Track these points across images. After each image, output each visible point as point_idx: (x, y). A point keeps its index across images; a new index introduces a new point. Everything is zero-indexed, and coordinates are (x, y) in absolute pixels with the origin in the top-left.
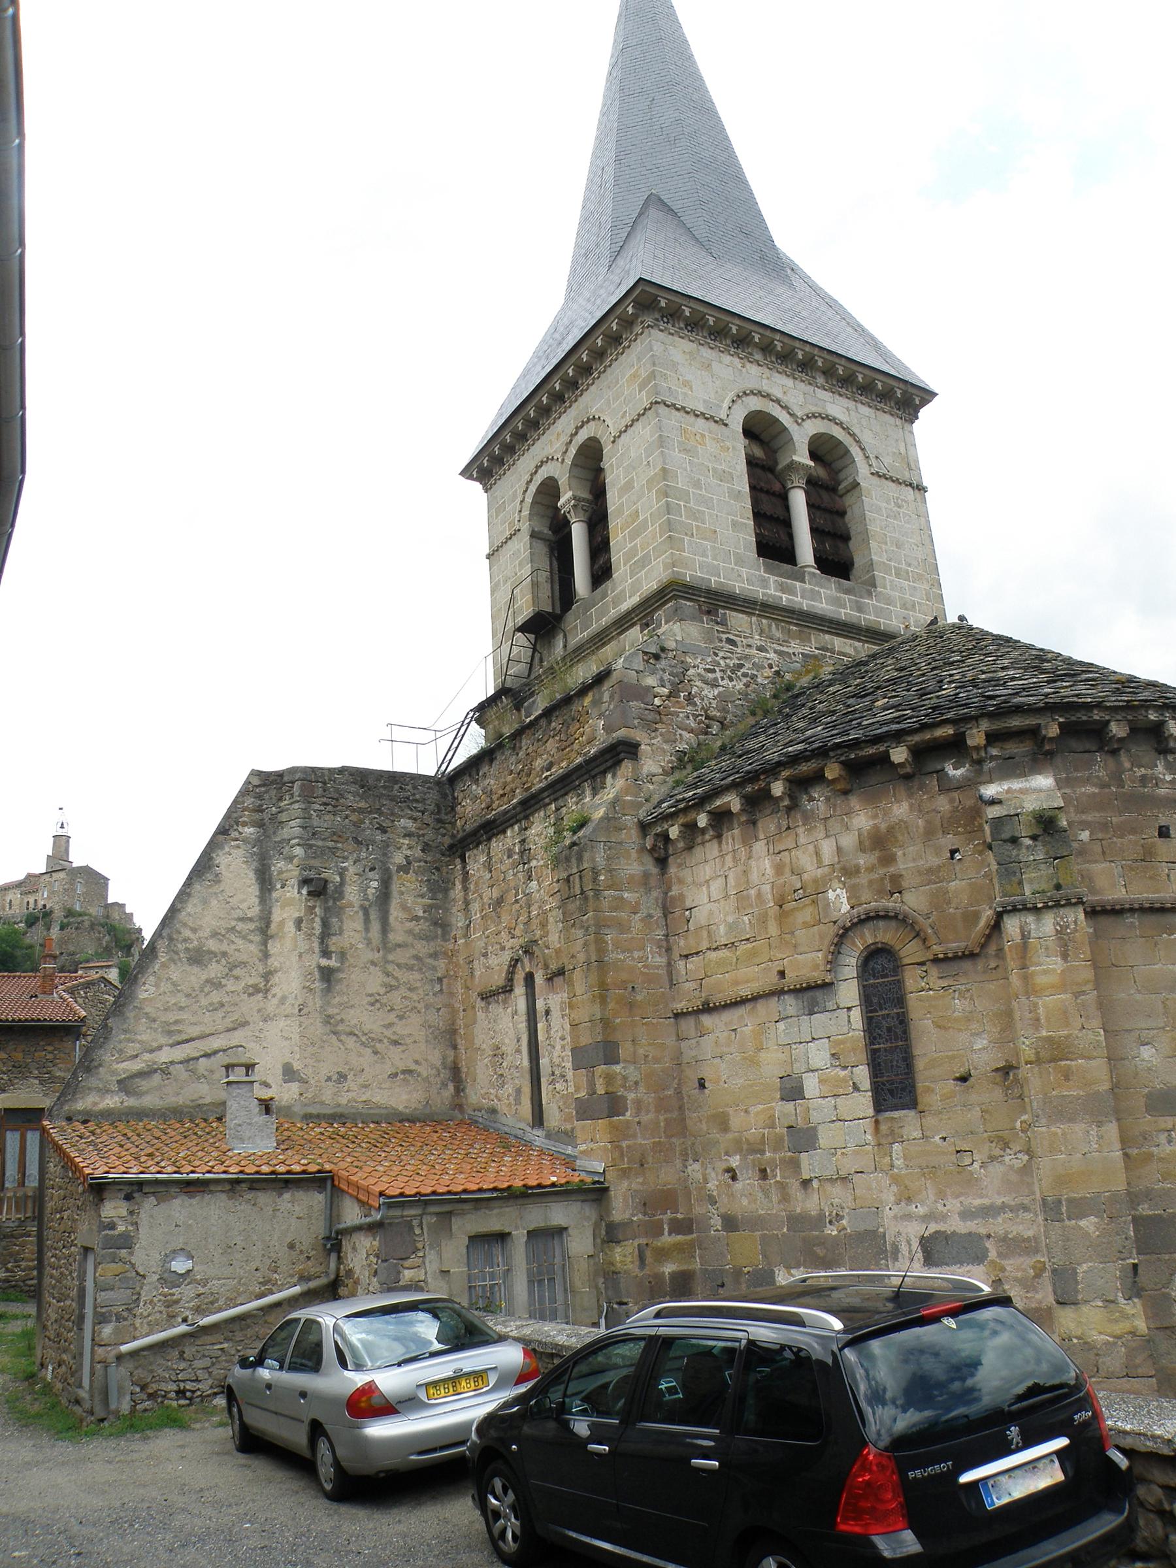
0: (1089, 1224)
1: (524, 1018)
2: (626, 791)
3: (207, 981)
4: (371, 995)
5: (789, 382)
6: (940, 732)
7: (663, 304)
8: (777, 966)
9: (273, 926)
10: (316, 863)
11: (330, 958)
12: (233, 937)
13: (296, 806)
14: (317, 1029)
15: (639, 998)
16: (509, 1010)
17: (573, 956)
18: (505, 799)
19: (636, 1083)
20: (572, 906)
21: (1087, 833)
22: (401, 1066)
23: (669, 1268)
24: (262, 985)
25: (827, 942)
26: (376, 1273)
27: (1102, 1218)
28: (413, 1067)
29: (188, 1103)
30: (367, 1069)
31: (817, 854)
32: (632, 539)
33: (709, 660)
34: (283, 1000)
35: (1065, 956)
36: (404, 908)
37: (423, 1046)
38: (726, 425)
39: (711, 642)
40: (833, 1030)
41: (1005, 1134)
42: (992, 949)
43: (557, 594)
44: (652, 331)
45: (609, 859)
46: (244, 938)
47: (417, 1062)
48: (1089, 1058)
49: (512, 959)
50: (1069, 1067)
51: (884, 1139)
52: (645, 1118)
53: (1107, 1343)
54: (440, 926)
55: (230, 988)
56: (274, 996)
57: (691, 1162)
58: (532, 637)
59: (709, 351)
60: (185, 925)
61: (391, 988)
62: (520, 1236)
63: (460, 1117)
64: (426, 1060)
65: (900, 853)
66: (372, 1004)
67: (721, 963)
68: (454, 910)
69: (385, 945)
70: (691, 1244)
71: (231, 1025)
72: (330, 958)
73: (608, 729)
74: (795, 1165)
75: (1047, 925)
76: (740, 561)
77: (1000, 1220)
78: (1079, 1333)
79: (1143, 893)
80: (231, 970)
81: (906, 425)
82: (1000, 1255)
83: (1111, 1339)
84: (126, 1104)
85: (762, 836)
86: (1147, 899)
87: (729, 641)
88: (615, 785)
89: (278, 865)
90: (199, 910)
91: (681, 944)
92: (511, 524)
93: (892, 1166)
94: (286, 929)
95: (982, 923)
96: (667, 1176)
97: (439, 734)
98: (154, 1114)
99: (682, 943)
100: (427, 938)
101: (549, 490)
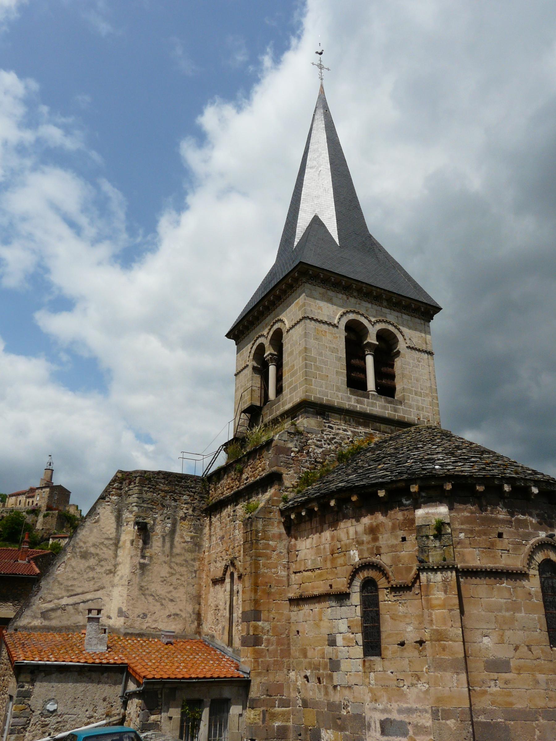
0: (451, 723)
1: (229, 593)
2: (275, 495)
3: (88, 567)
4: (162, 577)
5: (369, 305)
7: (311, 273)
8: (329, 582)
9: (121, 543)
10: (143, 515)
11: (145, 559)
12: (102, 547)
13: (136, 488)
14: (136, 592)
15: (273, 590)
17: (246, 569)
18: (229, 490)
19: (268, 631)
20: (247, 546)
21: (463, 534)
22: (173, 612)
23: (277, 724)
24: (113, 570)
25: (348, 575)
27: (457, 721)
28: (179, 612)
29: (73, 624)
30: (157, 612)
31: (348, 533)
33: (319, 435)
34: (122, 577)
35: (445, 592)
36: (182, 537)
39: (321, 427)
40: (349, 615)
41: (419, 673)
43: (263, 395)
45: (264, 526)
46: (107, 547)
47: (181, 610)
48: (455, 641)
49: (226, 565)
50: (445, 644)
51: (368, 668)
52: (271, 648)
54: (197, 545)
55: (98, 570)
56: (118, 575)
57: (291, 670)
59: (332, 292)
60: (81, 540)
61: (172, 574)
62: (207, 701)
63: (199, 638)
65: (380, 537)
66: (162, 582)
67: (309, 577)
68: (205, 539)
69: (171, 554)
70: (288, 713)
71: (96, 588)
72: (145, 559)
73: (270, 466)
74: (331, 677)
75: (439, 577)
76: (338, 389)
77: (415, 716)
80: (99, 562)
81: (426, 323)
82: (414, 733)
84: (43, 624)
85: (327, 522)
86: (489, 567)
88: (270, 492)
89: (126, 515)
90: (88, 533)
91: (294, 567)
93: (370, 683)
94: (126, 545)
96: (279, 677)
97: (204, 457)
98: (56, 630)
99: (294, 567)
101: (261, 348)
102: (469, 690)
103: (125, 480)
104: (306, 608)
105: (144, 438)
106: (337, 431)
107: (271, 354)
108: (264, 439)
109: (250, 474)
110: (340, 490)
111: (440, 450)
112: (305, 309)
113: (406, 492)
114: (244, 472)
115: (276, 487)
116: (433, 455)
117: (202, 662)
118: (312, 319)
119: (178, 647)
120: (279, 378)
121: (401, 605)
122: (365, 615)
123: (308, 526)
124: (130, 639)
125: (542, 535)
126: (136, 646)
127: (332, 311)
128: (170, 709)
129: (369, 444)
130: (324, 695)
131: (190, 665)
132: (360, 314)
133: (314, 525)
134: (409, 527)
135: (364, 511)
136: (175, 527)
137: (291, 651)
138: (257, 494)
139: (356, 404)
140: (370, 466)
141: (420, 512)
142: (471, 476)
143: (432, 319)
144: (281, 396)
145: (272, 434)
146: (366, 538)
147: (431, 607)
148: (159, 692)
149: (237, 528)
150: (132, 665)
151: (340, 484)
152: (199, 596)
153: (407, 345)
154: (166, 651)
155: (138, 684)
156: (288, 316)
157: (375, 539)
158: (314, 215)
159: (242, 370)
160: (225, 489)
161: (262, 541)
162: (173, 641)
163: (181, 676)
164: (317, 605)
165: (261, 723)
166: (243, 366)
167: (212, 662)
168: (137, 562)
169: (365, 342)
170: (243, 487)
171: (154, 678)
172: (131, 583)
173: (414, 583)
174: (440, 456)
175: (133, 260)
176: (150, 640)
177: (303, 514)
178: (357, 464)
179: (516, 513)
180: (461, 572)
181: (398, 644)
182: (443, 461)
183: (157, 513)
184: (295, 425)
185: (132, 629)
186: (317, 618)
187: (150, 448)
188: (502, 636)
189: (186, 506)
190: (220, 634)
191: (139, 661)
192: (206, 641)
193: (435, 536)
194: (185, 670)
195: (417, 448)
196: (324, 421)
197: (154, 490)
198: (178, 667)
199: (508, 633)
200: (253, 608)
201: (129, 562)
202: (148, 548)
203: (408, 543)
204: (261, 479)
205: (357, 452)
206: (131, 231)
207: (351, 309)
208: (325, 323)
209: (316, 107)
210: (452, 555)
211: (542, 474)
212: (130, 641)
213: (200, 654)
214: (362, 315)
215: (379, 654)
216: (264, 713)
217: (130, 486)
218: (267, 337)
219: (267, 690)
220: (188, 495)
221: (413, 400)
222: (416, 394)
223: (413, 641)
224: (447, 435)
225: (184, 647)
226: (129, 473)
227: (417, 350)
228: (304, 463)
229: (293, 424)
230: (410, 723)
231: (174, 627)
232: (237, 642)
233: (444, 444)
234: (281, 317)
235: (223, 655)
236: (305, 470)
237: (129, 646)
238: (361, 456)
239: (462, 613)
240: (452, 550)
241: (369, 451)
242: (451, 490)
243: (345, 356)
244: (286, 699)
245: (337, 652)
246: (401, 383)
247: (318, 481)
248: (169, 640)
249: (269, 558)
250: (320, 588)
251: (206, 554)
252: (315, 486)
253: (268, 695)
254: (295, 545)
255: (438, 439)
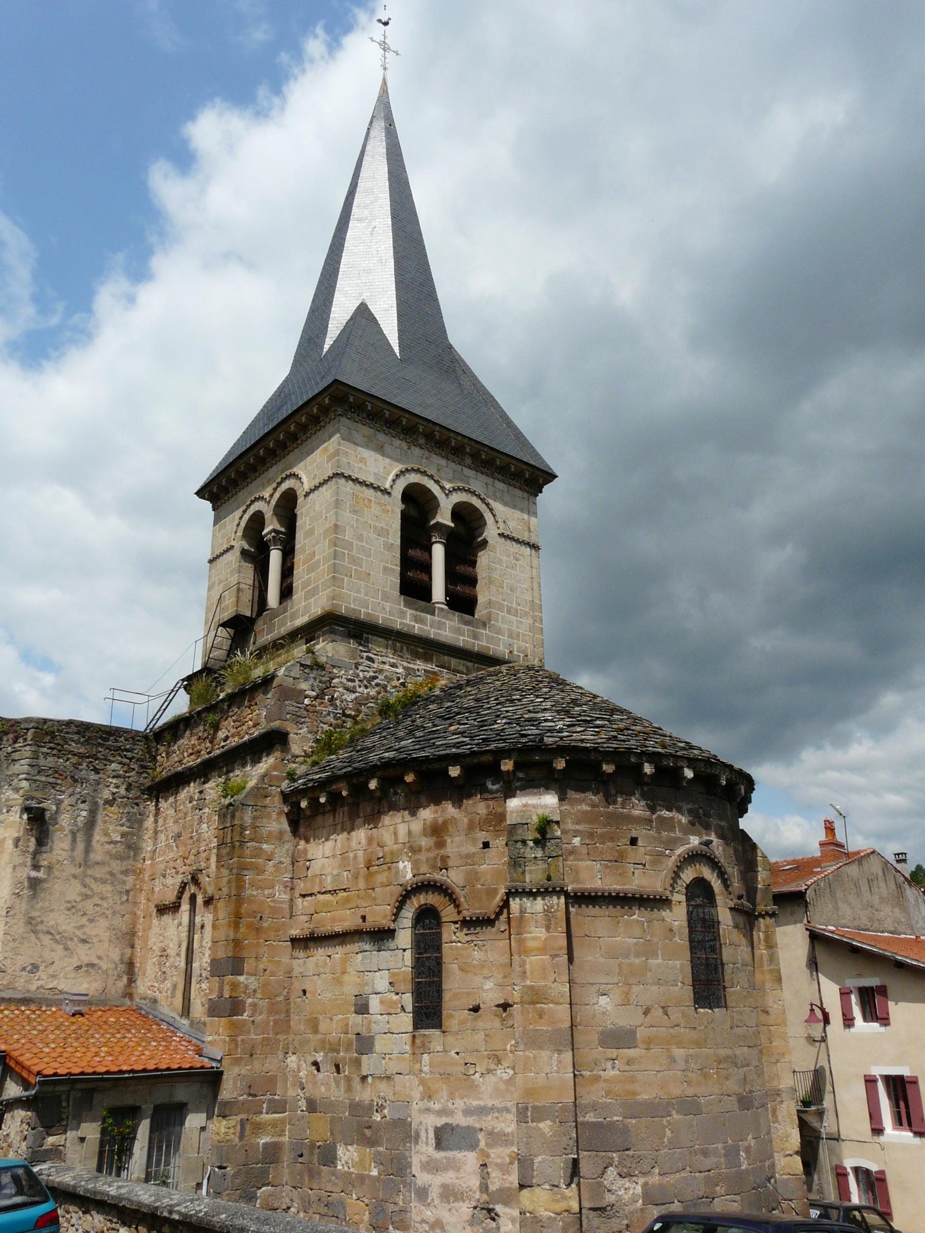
0: (545, 1126)
1: (186, 929)
2: (274, 767)
4: (69, 902)
5: (443, 462)
6: (484, 758)
7: (351, 400)
8: (361, 912)
10: (38, 795)
11: (39, 871)
13: (28, 748)
14: (20, 928)
15: (265, 925)
16: (176, 921)
17: (220, 889)
18: (192, 757)
19: (255, 991)
20: (224, 851)
21: (578, 839)
22: (86, 960)
25: (394, 900)
26: (25, 1138)
27: (555, 1122)
28: (95, 961)
31: (395, 834)
32: (309, 573)
33: (351, 672)
35: (548, 928)
36: (106, 834)
37: (106, 944)
38: (389, 494)
39: (354, 658)
40: (392, 965)
42: (503, 918)
43: (256, 599)
44: (342, 419)
45: (255, 818)
47: (99, 958)
49: (183, 882)
50: (543, 1009)
51: (418, 1048)
52: (259, 1018)
53: (549, 1218)
54: (132, 847)
57: (290, 1054)
58: (231, 631)
61: (86, 897)
62: (148, 1108)
63: (129, 1003)
64: (107, 956)
65: (449, 841)
66: (69, 910)
67: (327, 903)
68: (146, 837)
69: (86, 863)
70: (283, 1121)
72: (39, 871)
73: (269, 719)
74: (357, 1063)
75: (539, 904)
76: (385, 597)
77: (490, 1118)
78: (531, 1210)
79: (614, 885)
81: (531, 498)
82: (487, 1144)
83: (553, 1215)
87: (370, 659)
88: (267, 763)
92: (229, 540)
93: (421, 1071)
94: (6, 846)
95: (498, 898)
96: (270, 1065)
99: (302, 885)
100: (122, 858)
101: (257, 520)
102: (575, 1075)
103: (6, 733)
104: (320, 954)
105: (35, 659)
106: (381, 666)
107: (274, 531)
108: (258, 673)
109: (233, 731)
110: (387, 764)
111: (548, 705)
112: (338, 461)
113: (493, 770)
114: (221, 726)
115: (278, 754)
116: (537, 712)
117: (138, 1044)
118: (349, 478)
119: (94, 1019)
120: (287, 571)
121: (476, 948)
122: (418, 965)
123: (329, 819)
124: (7, 1009)
125: (695, 841)
126: (19, 1020)
127: (383, 467)
128: (83, 1125)
129: (430, 689)
130: (346, 1092)
131: (117, 1049)
132: (428, 475)
133: (339, 819)
134: (495, 826)
135: (423, 799)
136: (94, 817)
137: (292, 1023)
138: (244, 765)
139: (413, 623)
140: (435, 726)
141: (514, 803)
142: (595, 749)
143: (541, 492)
144: (289, 603)
145: (272, 666)
146: (425, 842)
147: (524, 952)
148: (64, 1097)
149: (205, 820)
150: (15, 1054)
151: (386, 755)
152: (133, 934)
153: (499, 532)
154: (74, 1028)
155: (26, 1085)
156: (309, 468)
157: (441, 844)
158: (360, 302)
159: (222, 554)
160: (186, 754)
161: (249, 844)
162: (83, 1009)
163: (104, 1070)
164: (339, 949)
165: (237, 1140)
166: (225, 547)
167: (155, 1044)
168: (25, 875)
169: (432, 523)
170: (218, 752)
171: (55, 1074)
172: (12, 913)
173: (498, 914)
174: (548, 715)
175: (47, 357)
176: (44, 1009)
177: (322, 800)
178: (413, 722)
179: (658, 808)
180: (571, 897)
181: (470, 1010)
182: (553, 724)
183: (64, 792)
184: (313, 653)
185: (11, 991)
186: (338, 969)
187: (48, 679)
188: (627, 993)
189: (114, 781)
190: (167, 996)
191: (26, 1047)
192: (141, 1009)
193: (536, 842)
194: (110, 1058)
195: (512, 701)
196: (361, 648)
197: (60, 752)
198: (96, 1054)
199: (636, 989)
200: (230, 954)
201: (9, 876)
202: (45, 852)
203: (492, 852)
204: (252, 741)
205: (412, 702)
206: (41, 301)
207: (413, 466)
208: (370, 486)
209: (373, 117)
210: (561, 870)
211: (700, 749)
212: (6, 1012)
213: (133, 1031)
214: (431, 477)
215: (439, 1025)
216: (243, 1123)
217: (17, 745)
218: (269, 502)
219: (250, 1087)
220: (119, 763)
221: (504, 621)
222: (509, 612)
223: (493, 1004)
224: (557, 682)
225: (104, 1019)
226: (16, 723)
227: (515, 540)
228: (325, 716)
229: (310, 651)
230: (481, 1129)
231: (87, 986)
232: (198, 1009)
233: (553, 696)
234: (295, 470)
235: (172, 1032)
236: (326, 727)
237: (6, 1020)
238: (419, 708)
239: (571, 960)
240: (560, 864)
241: (433, 702)
242: (564, 769)
243: (399, 543)
244: (278, 1100)
245: (370, 1023)
246: (487, 593)
247: (346, 747)
248: (77, 1008)
249: (260, 871)
250: (346, 920)
251: (148, 862)
252: (343, 754)
253: (250, 1095)
254: (305, 851)
255: (545, 687)
